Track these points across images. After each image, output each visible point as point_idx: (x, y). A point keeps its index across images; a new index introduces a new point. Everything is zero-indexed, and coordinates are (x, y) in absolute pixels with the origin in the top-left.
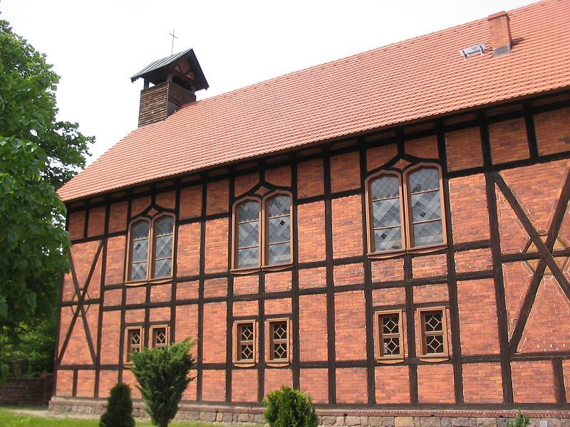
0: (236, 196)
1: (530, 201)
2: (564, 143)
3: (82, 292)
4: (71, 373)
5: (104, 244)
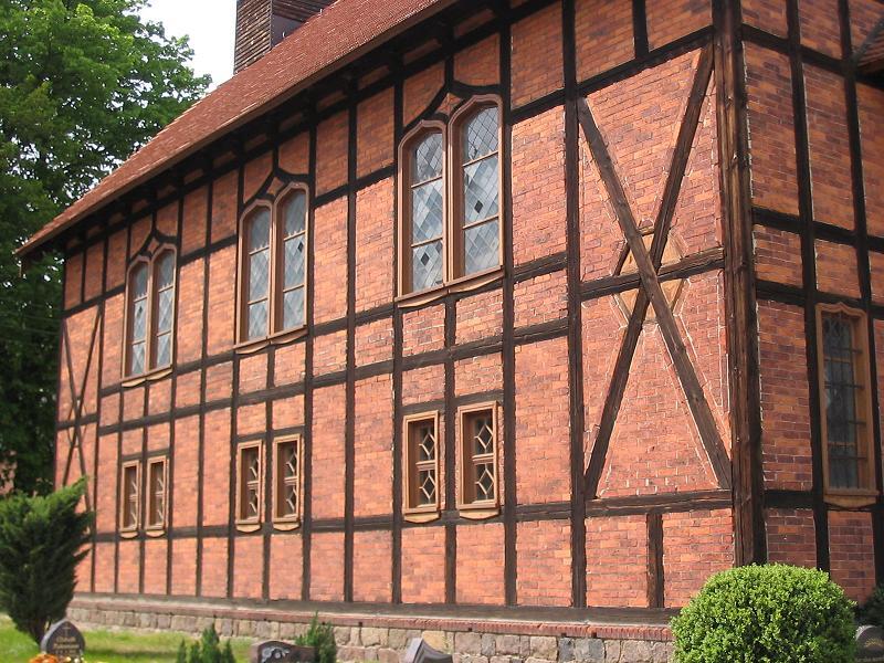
1: (630, 158)
2: (689, 13)
3: (648, 241)
4: (636, 528)
5: (577, 120)
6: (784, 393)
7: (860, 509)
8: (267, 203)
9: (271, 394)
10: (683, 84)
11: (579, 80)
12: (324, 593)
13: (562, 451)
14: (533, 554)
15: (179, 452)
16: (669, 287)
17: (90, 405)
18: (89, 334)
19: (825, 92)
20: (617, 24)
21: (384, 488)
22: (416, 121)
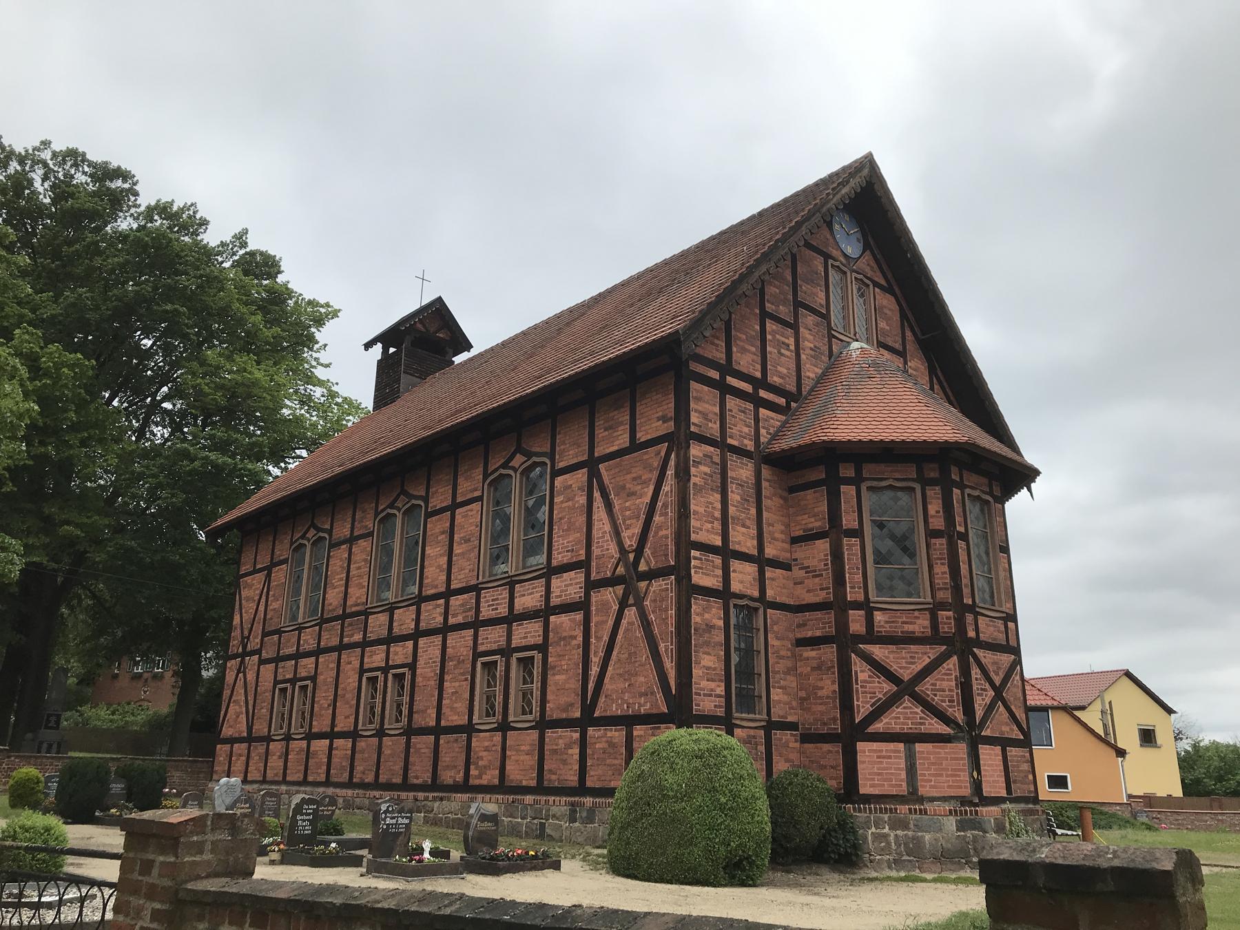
0: (758, 375)
3: (632, 556)
5: (269, 576)
6: (709, 654)
7: (756, 728)
8: (395, 512)
9: (512, 618)
10: (656, 464)
11: (596, 455)
12: (417, 778)
13: (576, 685)
14: (555, 751)
15: (321, 678)
16: (643, 585)
17: (254, 643)
18: (258, 592)
19: (742, 471)
20: (622, 423)
21: (462, 706)
22: (496, 470)
